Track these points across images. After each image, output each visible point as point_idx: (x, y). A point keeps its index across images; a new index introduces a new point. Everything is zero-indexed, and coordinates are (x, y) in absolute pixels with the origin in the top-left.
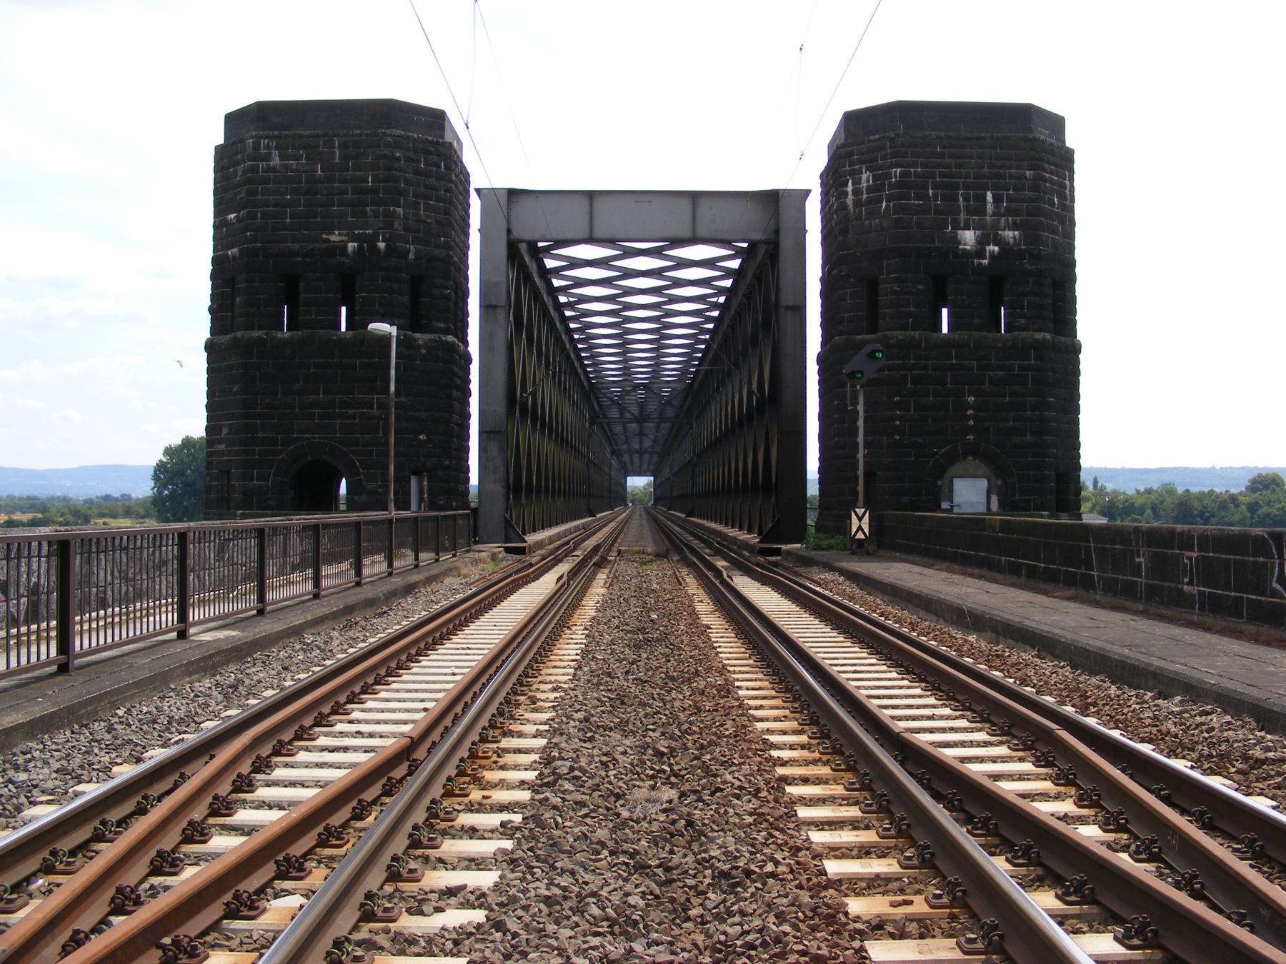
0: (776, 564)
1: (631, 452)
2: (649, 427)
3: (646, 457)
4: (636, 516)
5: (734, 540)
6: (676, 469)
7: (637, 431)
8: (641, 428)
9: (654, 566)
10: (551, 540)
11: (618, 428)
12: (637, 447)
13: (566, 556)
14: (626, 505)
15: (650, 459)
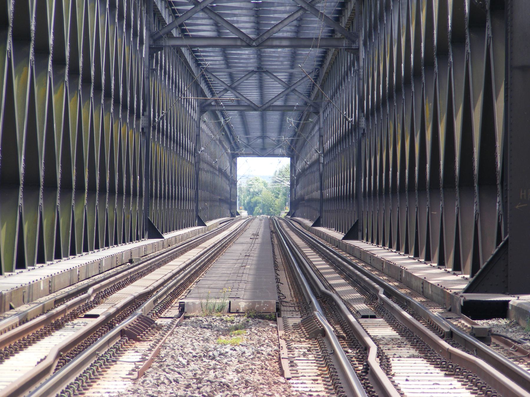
0: (485, 336)
1: (244, 107)
2: (278, 57)
3: (274, 117)
4: (246, 238)
5: (422, 287)
6: (328, 145)
7: (252, 64)
8: (260, 57)
9: (241, 338)
10: (51, 285)
11: (213, 59)
12: (253, 96)
13: (74, 316)
14: (234, 214)
15: (282, 120)
